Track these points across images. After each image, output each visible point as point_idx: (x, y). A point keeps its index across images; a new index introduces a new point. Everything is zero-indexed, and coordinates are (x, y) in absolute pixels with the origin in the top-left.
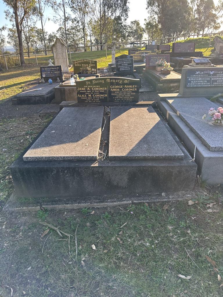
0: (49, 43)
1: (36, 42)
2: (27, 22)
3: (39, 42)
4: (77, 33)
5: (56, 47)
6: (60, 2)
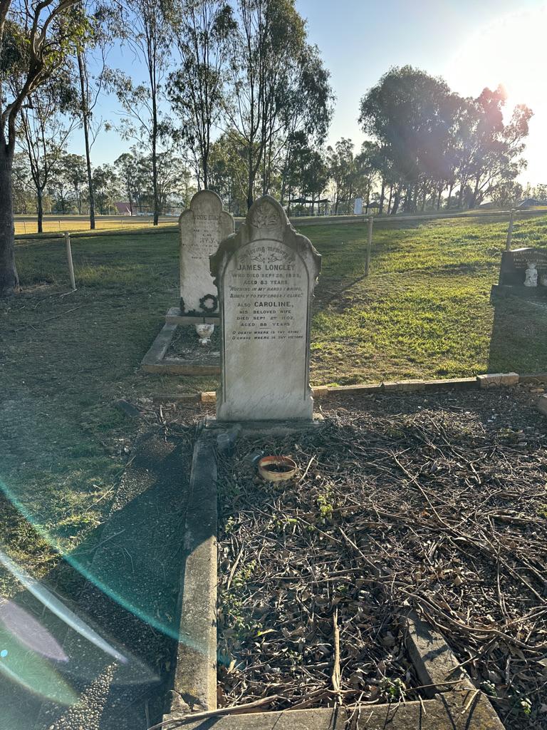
1: (61, 185)
2: (43, 131)
6: (141, 84)
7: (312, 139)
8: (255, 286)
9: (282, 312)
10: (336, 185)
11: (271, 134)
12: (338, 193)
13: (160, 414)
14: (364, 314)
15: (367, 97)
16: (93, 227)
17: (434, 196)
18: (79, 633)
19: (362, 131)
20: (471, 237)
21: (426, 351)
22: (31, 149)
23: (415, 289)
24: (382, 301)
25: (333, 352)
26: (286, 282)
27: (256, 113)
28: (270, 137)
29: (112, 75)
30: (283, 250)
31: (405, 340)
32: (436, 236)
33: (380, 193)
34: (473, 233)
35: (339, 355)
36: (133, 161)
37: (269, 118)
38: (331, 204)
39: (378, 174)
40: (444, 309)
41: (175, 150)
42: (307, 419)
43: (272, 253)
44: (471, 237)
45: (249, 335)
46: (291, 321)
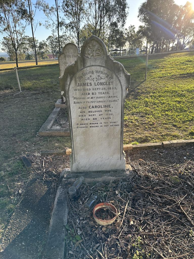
0: (40, 49)
1: (28, 49)
3: (31, 49)
4: (64, 41)
5: (80, 78)
6: (52, 6)
7: (119, 25)
8: (89, 96)
9: (106, 111)
10: (129, 43)
11: (103, 24)
12: (130, 47)
13: (42, 165)
14: (146, 99)
15: (141, 7)
16: (37, 64)
17: (167, 46)
18: (142, 7)
19: (139, 21)
20: (188, 61)
21: (181, 120)
22: (12, 35)
23: (168, 86)
24: (154, 92)
25: (133, 121)
26: (108, 92)
27: (97, 15)
28: (103, 25)
29: (41, 3)
30: (105, 72)
31: (169, 113)
32: (173, 61)
33: (146, 46)
34: (189, 59)
35: (137, 123)
36: (53, 39)
37: (102, 17)
38: (127, 51)
39: (145, 39)
40: (184, 96)
41: (67, 32)
42: (122, 170)
43: (98, 74)
44: (188, 61)
45: (86, 126)
46: (111, 116)
